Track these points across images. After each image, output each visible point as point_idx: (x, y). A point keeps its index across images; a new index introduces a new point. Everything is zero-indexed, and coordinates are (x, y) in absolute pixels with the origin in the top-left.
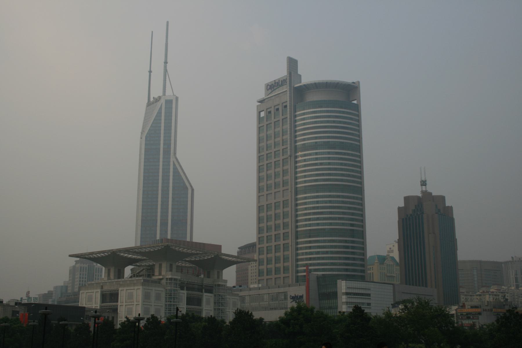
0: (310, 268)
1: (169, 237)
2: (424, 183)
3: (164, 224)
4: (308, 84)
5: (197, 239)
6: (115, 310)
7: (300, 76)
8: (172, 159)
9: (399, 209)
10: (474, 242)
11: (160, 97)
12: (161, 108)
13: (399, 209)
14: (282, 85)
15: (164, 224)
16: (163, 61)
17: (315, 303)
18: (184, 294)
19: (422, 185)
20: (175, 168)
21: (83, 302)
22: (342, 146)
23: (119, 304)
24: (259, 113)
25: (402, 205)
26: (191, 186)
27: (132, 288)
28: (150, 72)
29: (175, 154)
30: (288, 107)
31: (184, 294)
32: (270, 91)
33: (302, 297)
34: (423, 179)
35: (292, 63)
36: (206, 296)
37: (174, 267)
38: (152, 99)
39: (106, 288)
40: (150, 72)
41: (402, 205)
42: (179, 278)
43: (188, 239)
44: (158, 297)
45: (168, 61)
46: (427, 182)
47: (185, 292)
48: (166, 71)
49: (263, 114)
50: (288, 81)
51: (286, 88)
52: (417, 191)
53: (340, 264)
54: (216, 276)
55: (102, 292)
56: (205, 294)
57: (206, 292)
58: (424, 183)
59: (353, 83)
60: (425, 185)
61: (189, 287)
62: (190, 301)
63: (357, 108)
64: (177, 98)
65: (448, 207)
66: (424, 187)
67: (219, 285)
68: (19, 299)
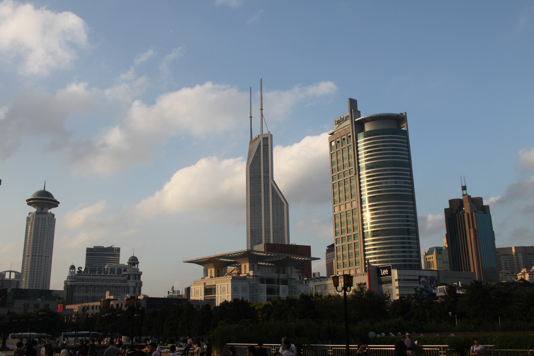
0: (370, 261)
1: (272, 242)
2: (464, 188)
3: (267, 231)
4: (374, 116)
5: (50, 289)
6: (214, 300)
7: (360, 112)
8: (271, 182)
9: (446, 210)
10: (509, 232)
11: (259, 136)
12: (259, 146)
13: (446, 210)
14: (346, 120)
15: (267, 231)
16: (260, 108)
17: (247, 298)
18: (264, 286)
19: (463, 190)
20: (273, 187)
21: (193, 297)
22: (395, 164)
23: (216, 295)
24: (331, 143)
25: (448, 206)
26: (286, 202)
27: (225, 284)
28: (251, 117)
29: (272, 177)
30: (351, 137)
31: (264, 286)
32: (337, 125)
33: (365, 284)
34: (464, 185)
35: (353, 103)
36: (282, 287)
37: (256, 266)
38: (254, 138)
39: (207, 284)
40: (251, 117)
41: (448, 206)
42: (259, 275)
43: (286, 243)
44: (244, 290)
45: (259, 111)
46: (467, 187)
47: (265, 285)
48: (262, 115)
49: (333, 144)
50: (350, 116)
51: (348, 122)
52: (458, 195)
53: (399, 257)
54: (289, 272)
55: (205, 287)
56: (281, 286)
57: (282, 284)
58: (464, 188)
59: (402, 114)
60: (466, 190)
61: (269, 281)
62: (270, 291)
63: (406, 133)
64: (271, 136)
65: (66, 286)
66: (464, 191)
67: (292, 279)
68: (183, 292)
